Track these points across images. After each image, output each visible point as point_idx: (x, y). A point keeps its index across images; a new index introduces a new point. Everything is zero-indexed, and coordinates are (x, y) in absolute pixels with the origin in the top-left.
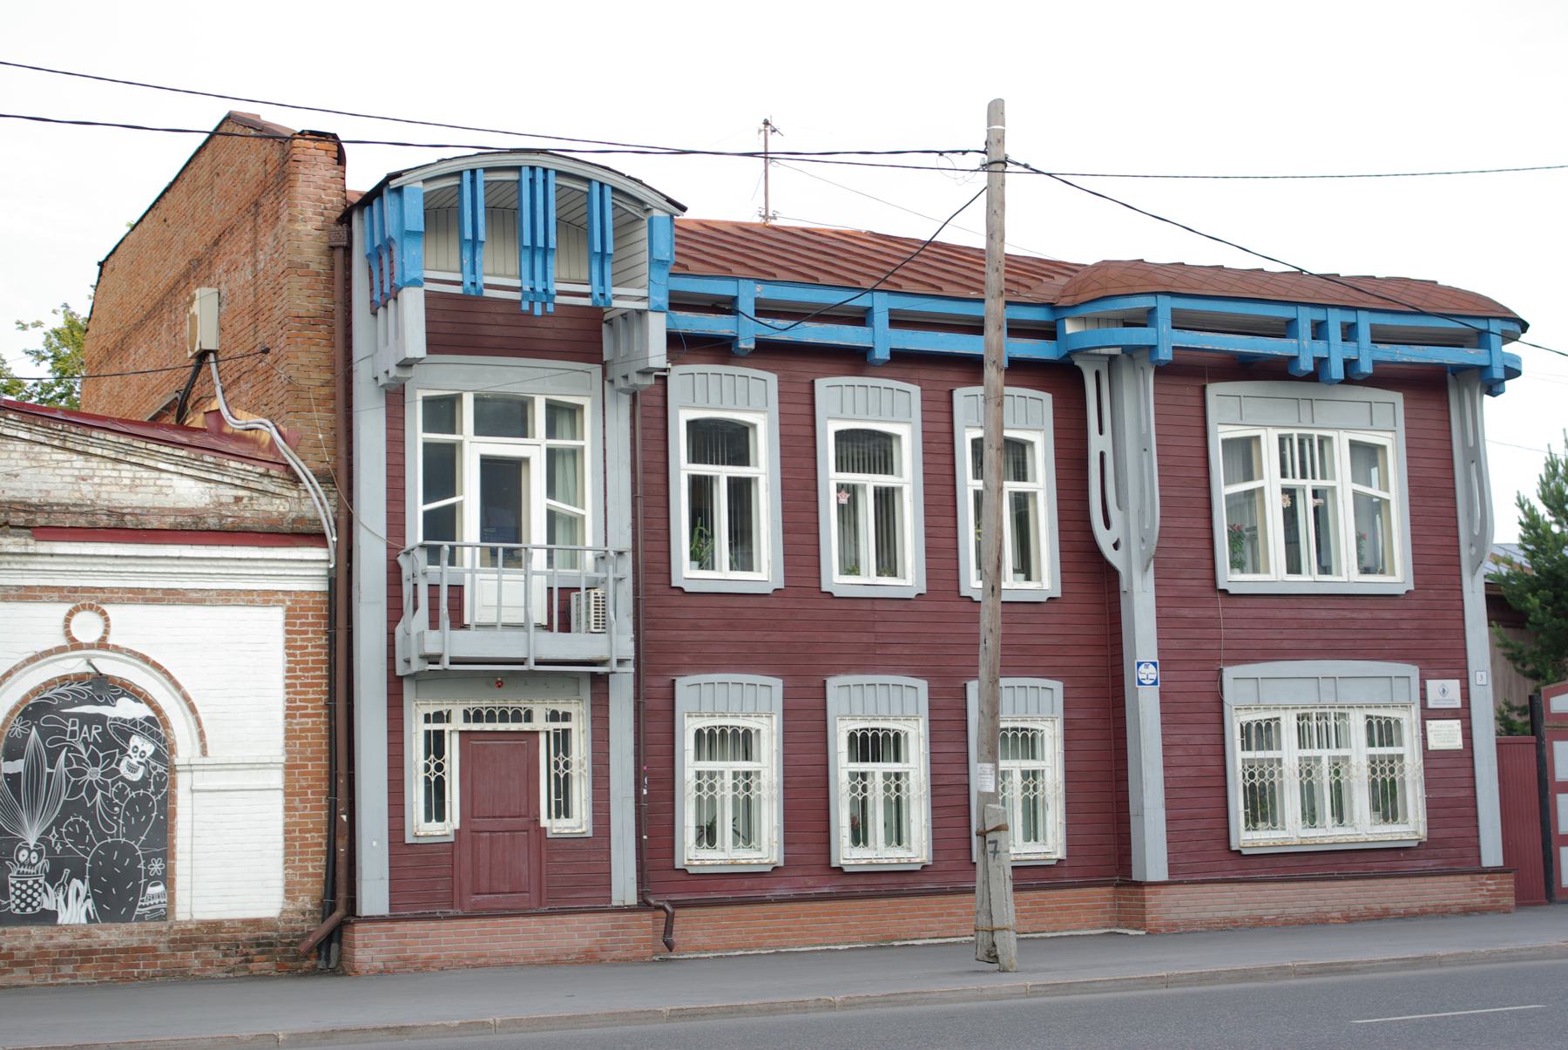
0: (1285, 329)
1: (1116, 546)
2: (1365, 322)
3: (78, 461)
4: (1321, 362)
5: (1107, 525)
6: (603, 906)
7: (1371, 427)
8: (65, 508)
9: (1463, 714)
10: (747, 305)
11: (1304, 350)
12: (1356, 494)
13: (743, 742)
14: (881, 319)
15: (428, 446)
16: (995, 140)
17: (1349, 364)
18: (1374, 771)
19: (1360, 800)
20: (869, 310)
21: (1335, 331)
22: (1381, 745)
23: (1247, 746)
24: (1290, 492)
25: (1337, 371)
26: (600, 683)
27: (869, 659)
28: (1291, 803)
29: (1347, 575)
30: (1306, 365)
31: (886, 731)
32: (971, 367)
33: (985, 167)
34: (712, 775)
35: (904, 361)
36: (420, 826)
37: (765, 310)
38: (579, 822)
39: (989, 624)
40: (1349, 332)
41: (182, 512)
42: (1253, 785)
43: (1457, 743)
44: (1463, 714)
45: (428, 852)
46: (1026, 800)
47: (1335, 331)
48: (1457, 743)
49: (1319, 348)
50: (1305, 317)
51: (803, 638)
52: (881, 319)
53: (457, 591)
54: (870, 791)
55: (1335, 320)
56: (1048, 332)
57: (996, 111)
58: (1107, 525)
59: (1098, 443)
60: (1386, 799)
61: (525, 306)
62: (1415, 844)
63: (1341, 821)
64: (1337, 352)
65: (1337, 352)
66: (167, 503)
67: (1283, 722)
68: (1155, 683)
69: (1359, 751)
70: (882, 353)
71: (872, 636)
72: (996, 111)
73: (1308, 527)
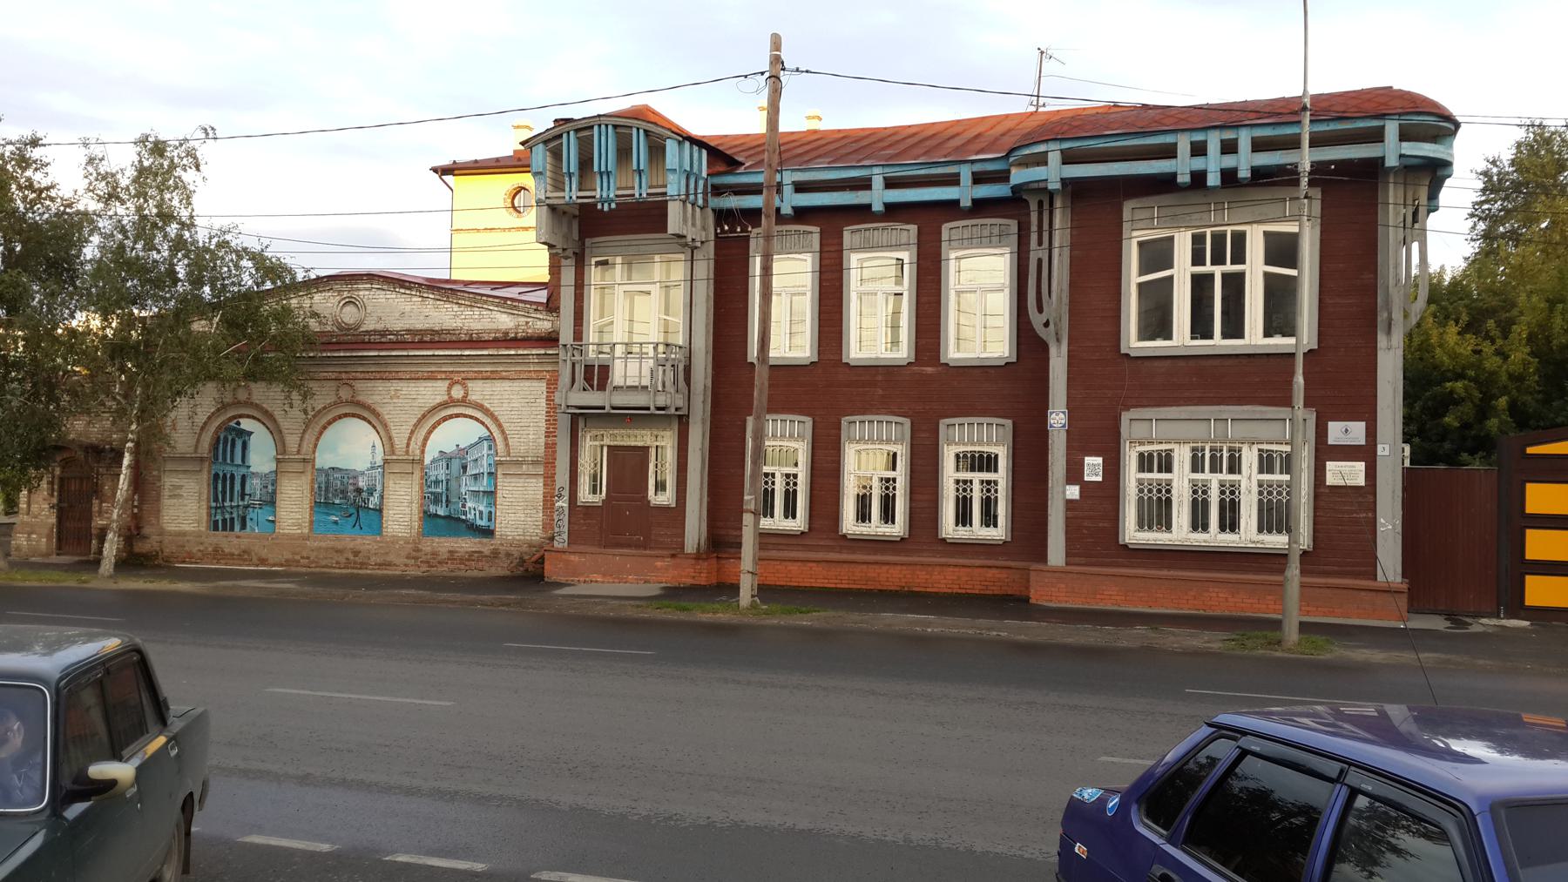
0: (1169, 152)
1: (1047, 324)
2: (1244, 138)
3: (456, 308)
4: (1199, 178)
5: (1040, 310)
6: (677, 551)
7: (1283, 219)
8: (448, 332)
9: (1366, 453)
10: (788, 190)
11: (1182, 166)
12: (1267, 275)
13: (988, 463)
14: (878, 182)
16: (777, 61)
17: (1229, 176)
19: (1181, 515)
20: (958, 175)
21: (1214, 147)
22: (1160, 471)
23: (1141, 469)
25: (1213, 180)
26: (683, 421)
28: (1181, 515)
30: (1184, 178)
31: (981, 455)
34: (965, 482)
35: (894, 212)
36: (585, 495)
37: (800, 188)
38: (666, 498)
39: (761, 378)
40: (1229, 148)
41: (498, 331)
43: (1361, 481)
44: (1366, 453)
45: (589, 509)
46: (787, 492)
47: (1214, 147)
48: (1361, 481)
49: (1198, 164)
50: (1184, 143)
51: (925, 390)
52: (878, 182)
55: (1214, 141)
56: (1003, 177)
57: (776, 42)
58: (1040, 310)
59: (1036, 252)
60: (1274, 516)
64: (1214, 164)
65: (1214, 164)
66: (494, 326)
67: (1176, 455)
69: (1249, 480)
70: (877, 207)
71: (876, 388)
72: (776, 42)
73: (1218, 304)
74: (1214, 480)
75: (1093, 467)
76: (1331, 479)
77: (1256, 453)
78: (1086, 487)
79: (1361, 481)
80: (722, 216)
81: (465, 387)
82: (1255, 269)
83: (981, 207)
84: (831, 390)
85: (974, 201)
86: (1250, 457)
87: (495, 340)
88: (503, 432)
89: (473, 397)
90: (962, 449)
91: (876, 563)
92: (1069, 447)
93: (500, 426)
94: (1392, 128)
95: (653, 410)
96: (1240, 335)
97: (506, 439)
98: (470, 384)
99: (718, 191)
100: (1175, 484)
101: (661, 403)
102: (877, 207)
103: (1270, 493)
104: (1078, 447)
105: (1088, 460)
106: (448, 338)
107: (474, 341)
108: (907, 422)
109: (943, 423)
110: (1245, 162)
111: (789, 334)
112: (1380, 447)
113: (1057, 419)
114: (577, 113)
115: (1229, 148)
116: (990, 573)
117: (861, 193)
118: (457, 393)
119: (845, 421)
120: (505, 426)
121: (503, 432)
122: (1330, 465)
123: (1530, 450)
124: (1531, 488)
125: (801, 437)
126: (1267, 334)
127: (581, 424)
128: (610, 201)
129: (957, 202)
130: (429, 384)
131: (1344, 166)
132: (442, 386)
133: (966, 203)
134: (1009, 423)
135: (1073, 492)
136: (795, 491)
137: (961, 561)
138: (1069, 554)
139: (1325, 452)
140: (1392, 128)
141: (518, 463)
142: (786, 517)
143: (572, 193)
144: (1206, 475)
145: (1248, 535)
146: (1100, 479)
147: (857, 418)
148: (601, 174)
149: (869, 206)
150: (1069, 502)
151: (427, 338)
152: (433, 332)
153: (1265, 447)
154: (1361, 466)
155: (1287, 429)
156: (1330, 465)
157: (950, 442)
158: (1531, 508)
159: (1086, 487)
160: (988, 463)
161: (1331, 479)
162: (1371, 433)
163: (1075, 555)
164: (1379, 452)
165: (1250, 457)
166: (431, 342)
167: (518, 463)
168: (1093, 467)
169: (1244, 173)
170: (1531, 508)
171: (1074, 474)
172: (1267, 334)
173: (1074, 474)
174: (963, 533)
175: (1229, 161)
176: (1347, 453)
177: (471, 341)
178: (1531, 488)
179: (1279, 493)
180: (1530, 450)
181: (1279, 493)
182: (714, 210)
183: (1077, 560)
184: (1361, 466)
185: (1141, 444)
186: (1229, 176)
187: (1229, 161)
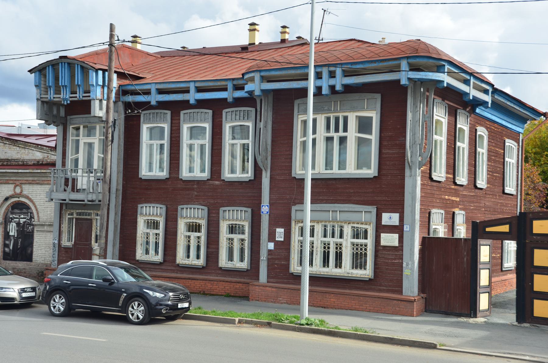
2: (339, 71)
3: (18, 148)
9: (398, 229)
13: (155, 225)
15: (370, 133)
17: (332, 88)
18: (337, 248)
19: (318, 259)
24: (329, 139)
27: (232, 202)
29: (351, 170)
32: (185, 104)
33: (109, 45)
42: (357, 253)
43: (396, 244)
44: (398, 229)
45: (67, 249)
51: (215, 193)
53: (74, 180)
54: (335, 247)
60: (359, 260)
61: (63, 103)
62: (368, 279)
63: (301, 265)
68: (267, 213)
69: (347, 244)
71: (192, 191)
74: (332, 241)
75: (280, 232)
76: (383, 243)
77: (350, 227)
78: (277, 243)
79: (396, 244)
80: (127, 105)
81: (21, 188)
82: (352, 134)
83: (238, 102)
84: (172, 191)
85: (196, 100)
86: (348, 231)
87: (34, 165)
88: (37, 210)
89: (25, 192)
90: (231, 222)
91: (189, 279)
92: (270, 224)
93: (35, 207)
94: (404, 65)
95: (86, 202)
96: (345, 169)
97: (38, 213)
98: (23, 186)
99: (125, 93)
100: (344, 245)
101: (90, 199)
102: (192, 102)
103: (357, 249)
104: (274, 223)
105: (278, 230)
106: (14, 163)
107: (24, 165)
108: (206, 209)
109: (222, 209)
110: (339, 82)
111: (152, 165)
112: (405, 226)
113: (265, 209)
114: (71, 54)
115: (332, 75)
116: (238, 286)
117: (185, 94)
118: (18, 190)
119: (180, 207)
120: (38, 207)
121: (37, 210)
122: (383, 235)
123: (488, 229)
124: (537, 252)
125: (161, 215)
126: (359, 167)
127: (64, 208)
128: (66, 99)
129: (226, 99)
130: (6, 186)
131: (276, 92)
132: (12, 187)
133: (230, 100)
134: (249, 210)
135: (271, 246)
136: (329, 252)
137: (242, 280)
138: (269, 277)
139: (380, 228)
140: (404, 65)
141: (43, 225)
142: (336, 267)
143: (51, 96)
144: (328, 239)
145: (347, 270)
146: (282, 240)
147: (185, 206)
148: (63, 86)
149: (188, 101)
150: (270, 251)
151: (5, 163)
152: (8, 160)
153: (356, 225)
154: (396, 236)
155: (365, 216)
156: (383, 235)
157: (224, 219)
158: (537, 263)
159: (277, 243)
160: (155, 225)
161: (383, 243)
162: (401, 219)
163: (273, 278)
164: (405, 229)
165: (348, 231)
166: (7, 165)
167: (43, 225)
168: (280, 232)
169: (338, 88)
170: (537, 263)
171: (272, 237)
172: (359, 167)
173: (272, 237)
174: (187, 262)
175: (332, 82)
176: (391, 229)
177: (23, 165)
178: (537, 252)
179: (361, 249)
180: (488, 229)
181: (361, 249)
182: (123, 102)
183: (272, 280)
184: (396, 236)
185: (353, 223)
186: (332, 88)
187: (332, 82)
